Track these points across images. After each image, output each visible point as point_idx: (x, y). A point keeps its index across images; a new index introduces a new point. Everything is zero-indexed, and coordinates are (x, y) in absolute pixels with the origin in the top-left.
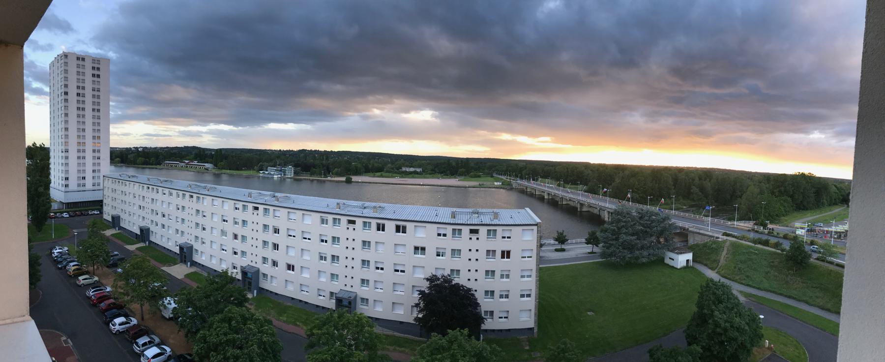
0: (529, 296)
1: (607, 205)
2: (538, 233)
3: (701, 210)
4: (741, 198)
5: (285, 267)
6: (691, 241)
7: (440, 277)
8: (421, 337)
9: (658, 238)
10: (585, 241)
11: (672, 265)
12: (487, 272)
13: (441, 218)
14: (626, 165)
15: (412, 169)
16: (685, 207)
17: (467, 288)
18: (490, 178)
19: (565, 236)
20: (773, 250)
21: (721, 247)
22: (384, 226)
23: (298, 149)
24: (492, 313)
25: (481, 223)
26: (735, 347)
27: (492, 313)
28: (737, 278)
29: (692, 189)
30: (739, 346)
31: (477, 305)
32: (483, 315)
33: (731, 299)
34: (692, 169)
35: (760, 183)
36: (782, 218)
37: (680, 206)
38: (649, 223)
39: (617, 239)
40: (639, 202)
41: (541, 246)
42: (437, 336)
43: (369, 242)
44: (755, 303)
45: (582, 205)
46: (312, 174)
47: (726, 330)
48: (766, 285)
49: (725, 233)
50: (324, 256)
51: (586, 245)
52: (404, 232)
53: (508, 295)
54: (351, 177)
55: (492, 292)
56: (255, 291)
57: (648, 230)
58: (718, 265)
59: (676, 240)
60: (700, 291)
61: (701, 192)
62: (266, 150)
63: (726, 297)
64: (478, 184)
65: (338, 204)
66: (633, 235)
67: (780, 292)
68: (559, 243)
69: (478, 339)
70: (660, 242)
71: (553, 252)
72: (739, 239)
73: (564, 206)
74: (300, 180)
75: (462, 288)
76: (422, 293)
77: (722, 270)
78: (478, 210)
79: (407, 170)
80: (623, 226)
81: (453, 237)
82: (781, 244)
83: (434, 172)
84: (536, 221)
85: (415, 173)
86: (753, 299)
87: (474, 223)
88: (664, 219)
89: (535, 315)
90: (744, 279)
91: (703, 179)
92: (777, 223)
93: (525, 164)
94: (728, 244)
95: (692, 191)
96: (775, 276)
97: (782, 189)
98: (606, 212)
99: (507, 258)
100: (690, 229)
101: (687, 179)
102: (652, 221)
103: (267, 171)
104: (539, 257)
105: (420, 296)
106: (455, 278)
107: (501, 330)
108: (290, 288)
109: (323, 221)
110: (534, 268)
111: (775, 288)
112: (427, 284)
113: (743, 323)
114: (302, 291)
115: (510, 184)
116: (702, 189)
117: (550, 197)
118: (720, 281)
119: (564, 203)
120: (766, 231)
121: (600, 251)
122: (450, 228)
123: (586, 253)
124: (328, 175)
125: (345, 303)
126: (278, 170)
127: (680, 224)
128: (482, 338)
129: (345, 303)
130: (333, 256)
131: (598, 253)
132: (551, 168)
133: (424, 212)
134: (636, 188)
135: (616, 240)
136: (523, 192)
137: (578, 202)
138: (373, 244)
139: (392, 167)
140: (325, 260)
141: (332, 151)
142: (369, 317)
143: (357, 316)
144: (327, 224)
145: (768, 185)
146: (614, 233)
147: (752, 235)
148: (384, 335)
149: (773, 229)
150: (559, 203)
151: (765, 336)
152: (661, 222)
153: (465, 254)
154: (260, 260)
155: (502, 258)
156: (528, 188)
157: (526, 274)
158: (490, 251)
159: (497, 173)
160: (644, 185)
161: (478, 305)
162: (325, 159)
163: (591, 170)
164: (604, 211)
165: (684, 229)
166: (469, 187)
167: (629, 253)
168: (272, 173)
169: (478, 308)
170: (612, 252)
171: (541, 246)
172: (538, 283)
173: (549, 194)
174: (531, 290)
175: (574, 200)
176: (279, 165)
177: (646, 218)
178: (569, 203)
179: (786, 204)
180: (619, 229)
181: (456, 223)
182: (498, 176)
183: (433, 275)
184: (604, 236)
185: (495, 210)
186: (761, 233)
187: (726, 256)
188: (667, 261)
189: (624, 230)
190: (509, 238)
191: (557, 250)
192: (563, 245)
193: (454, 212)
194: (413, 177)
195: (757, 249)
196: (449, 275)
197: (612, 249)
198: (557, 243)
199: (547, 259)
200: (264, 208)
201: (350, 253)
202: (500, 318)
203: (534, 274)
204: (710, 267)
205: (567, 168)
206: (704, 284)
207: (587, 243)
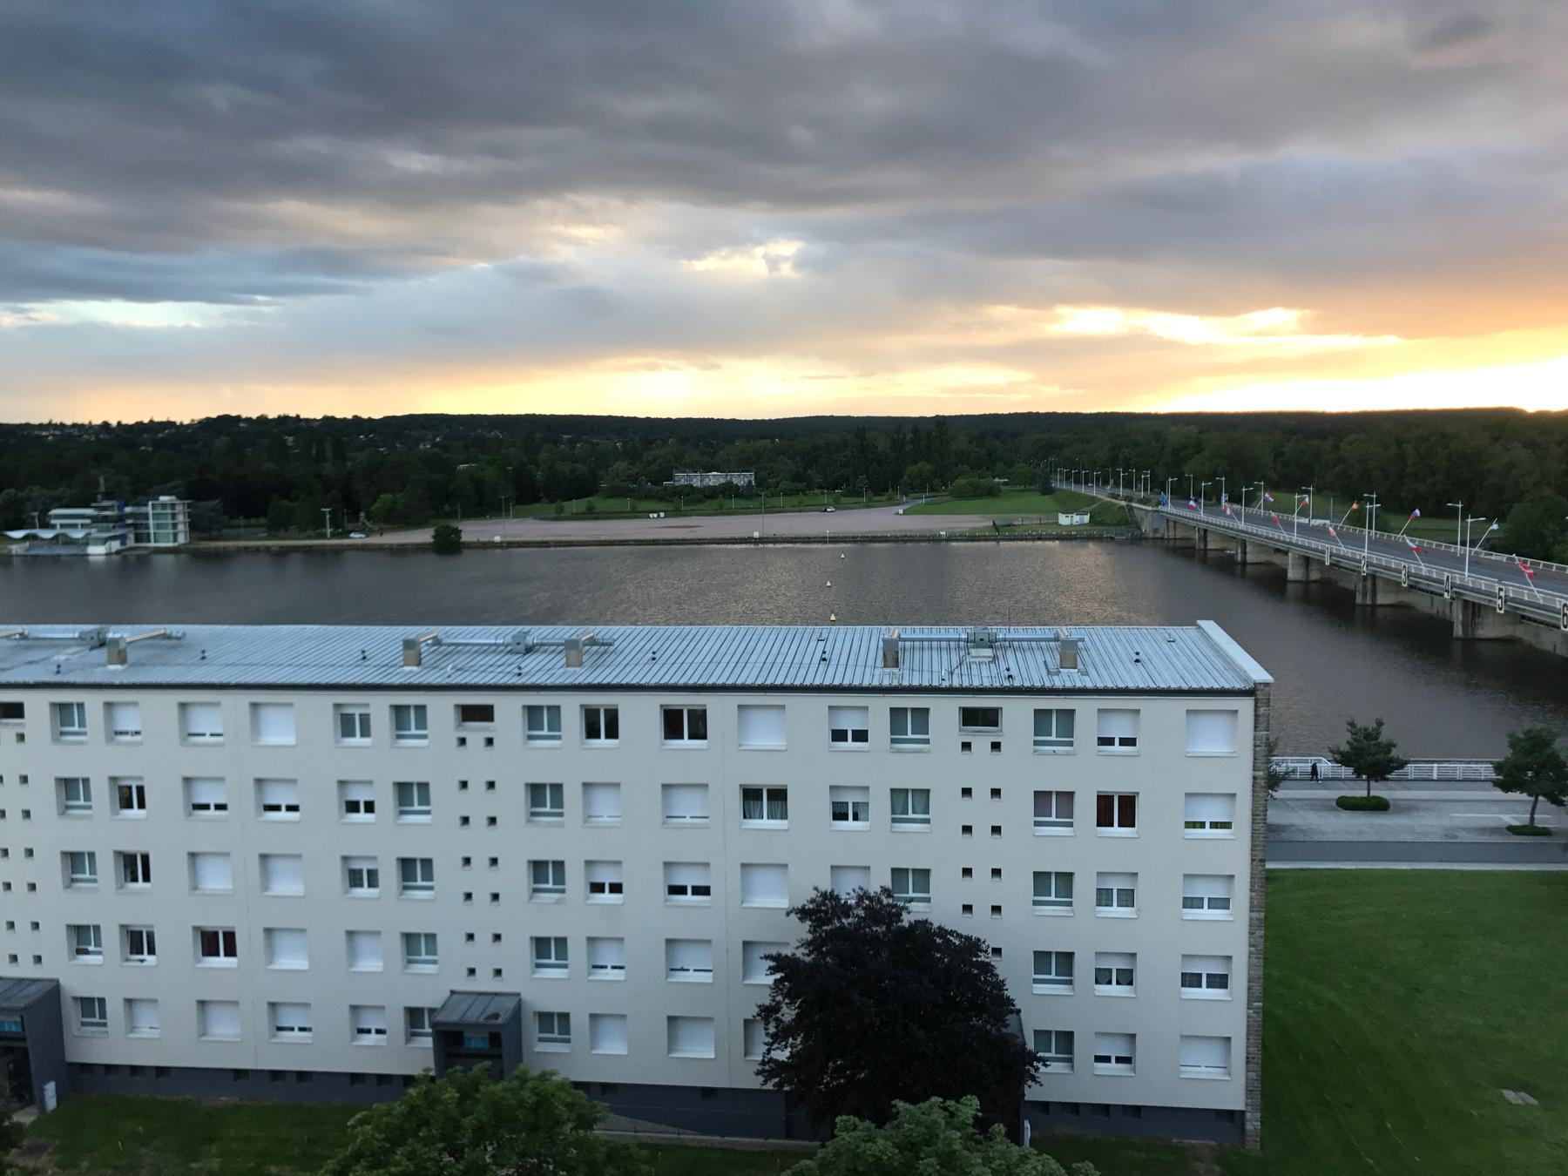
0: (1219, 981)
5: (189, 944)
7: (852, 902)
8: (789, 1136)
10: (1493, 776)
12: (1041, 879)
13: (841, 669)
15: (714, 479)
17: (959, 936)
18: (1036, 499)
22: (613, 716)
23: (200, 415)
25: (1006, 684)
31: (1002, 1006)
32: (1030, 1045)
41: (1274, 781)
42: (855, 1128)
43: (557, 788)
45: (1474, 610)
46: (278, 526)
50: (365, 866)
51: (1499, 794)
52: (699, 732)
54: (455, 524)
55: (1066, 960)
56: (50, 1088)
62: (28, 425)
65: (409, 645)
68: (1358, 772)
69: (1015, 1136)
73: (1313, 587)
74: (219, 558)
75: (939, 941)
76: (781, 963)
78: (994, 629)
79: (696, 483)
81: (893, 741)
83: (802, 485)
85: (728, 491)
87: (976, 683)
93: (1195, 429)
103: (46, 525)
105: (778, 976)
106: (911, 900)
107: (1106, 1109)
108: (224, 1028)
109: (347, 725)
112: (803, 930)
114: (280, 1029)
115: (1127, 520)
117: (1314, 576)
122: (880, 706)
123: (1495, 831)
124: (350, 526)
125: (476, 1042)
126: (105, 519)
128: (1028, 1134)
129: (473, 1045)
130: (407, 865)
133: (775, 651)
137: (1457, 596)
138: (572, 795)
139: (634, 471)
140: (373, 883)
141: (356, 418)
142: (577, 1085)
143: (529, 1085)
144: (366, 732)
148: (642, 1146)
150: (1359, 600)
154: (55, 943)
157: (1206, 891)
159: (1068, 478)
162: (329, 453)
166: (950, 539)
168: (78, 534)
169: (1010, 1018)
171: (1271, 781)
174: (1229, 958)
175: (1435, 587)
176: (108, 495)
181: (906, 683)
182: (1073, 488)
183: (824, 895)
185: (1065, 632)
190: (1130, 742)
191: (1346, 804)
192: (1380, 784)
194: (721, 511)
196: (885, 890)
198: (1346, 772)
200: (53, 705)
201: (479, 842)
202: (1099, 1059)
203: (1241, 893)
205: (1399, 443)
207: (1505, 786)
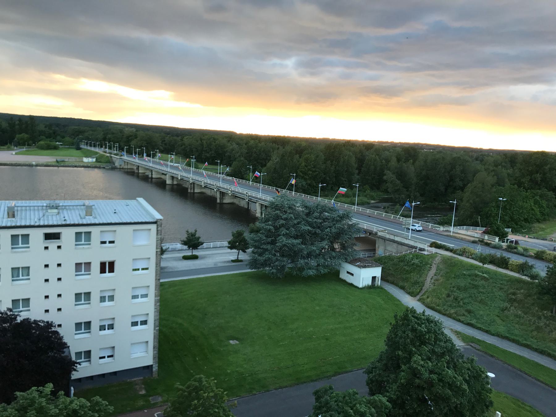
0: (144, 323)
1: (260, 195)
2: (157, 234)
3: (398, 206)
4: (462, 190)
6: (380, 251)
9: (332, 243)
10: (227, 245)
11: (351, 282)
14: (288, 137)
16: (373, 202)
17: (43, 322)
19: (199, 238)
20: (516, 275)
21: (427, 264)
24: (88, 354)
26: (445, 411)
27: (88, 354)
28: (452, 311)
29: (385, 175)
30: (450, 410)
32: (74, 358)
33: (440, 341)
34: (387, 145)
35: (496, 166)
36: (536, 225)
37: (365, 199)
38: (320, 221)
39: (273, 243)
40: (305, 192)
41: (163, 252)
44: (480, 353)
45: (223, 194)
47: (431, 384)
48: (502, 329)
49: (434, 243)
51: (229, 250)
53: (113, 325)
57: (318, 231)
58: (422, 289)
59: (358, 247)
60: (394, 322)
61: (399, 179)
63: (433, 336)
64: (55, 160)
66: (296, 237)
67: (525, 342)
68: (189, 247)
69: (68, 394)
70: (333, 249)
71: (180, 260)
72: (457, 254)
75: (34, 325)
77: (428, 297)
80: (283, 225)
82: (532, 267)
84: (154, 218)
86: (478, 347)
88: (342, 217)
89: (154, 348)
90: (464, 315)
91: (403, 160)
92: (526, 233)
94: (438, 259)
95: (385, 177)
96: (516, 316)
97: (538, 177)
98: (257, 204)
99: (109, 272)
100: (380, 234)
101: (378, 160)
102: (324, 219)
104: (158, 268)
106: (21, 311)
107: (103, 375)
110: (152, 282)
111: (516, 335)
113: (460, 378)
115: (110, 161)
116: (401, 175)
117: (175, 183)
118: (424, 312)
119: (196, 191)
120: (504, 245)
121: (249, 258)
123: (228, 262)
127: (365, 225)
128: (73, 392)
131: (246, 261)
132: (175, 138)
134: (301, 172)
135: (272, 244)
136: (132, 173)
145: (510, 171)
146: (269, 233)
147: (479, 249)
149: (517, 242)
150: (189, 191)
151: (495, 404)
152: (337, 221)
153: (38, 273)
155: (101, 272)
156: (140, 168)
158: (81, 264)
159: (87, 144)
160: (314, 167)
161: (64, 346)
163: (238, 144)
164: (256, 203)
165: (371, 233)
166: (37, 165)
167: (289, 261)
170: (265, 260)
171: (163, 252)
172: (158, 304)
173: (173, 178)
177: (316, 214)
178: (204, 190)
179: (544, 203)
180: (277, 228)
182: (89, 148)
184: (256, 239)
185: (87, 202)
186: (495, 247)
187: (435, 277)
188: (343, 276)
189: (284, 231)
191: (185, 258)
192: (196, 250)
193: (13, 207)
195: (488, 272)
196: (10, 310)
197: (267, 256)
198: (186, 247)
199: (171, 270)
203: (152, 292)
204: (409, 291)
205: (201, 140)
206: (400, 314)
207: (231, 248)
